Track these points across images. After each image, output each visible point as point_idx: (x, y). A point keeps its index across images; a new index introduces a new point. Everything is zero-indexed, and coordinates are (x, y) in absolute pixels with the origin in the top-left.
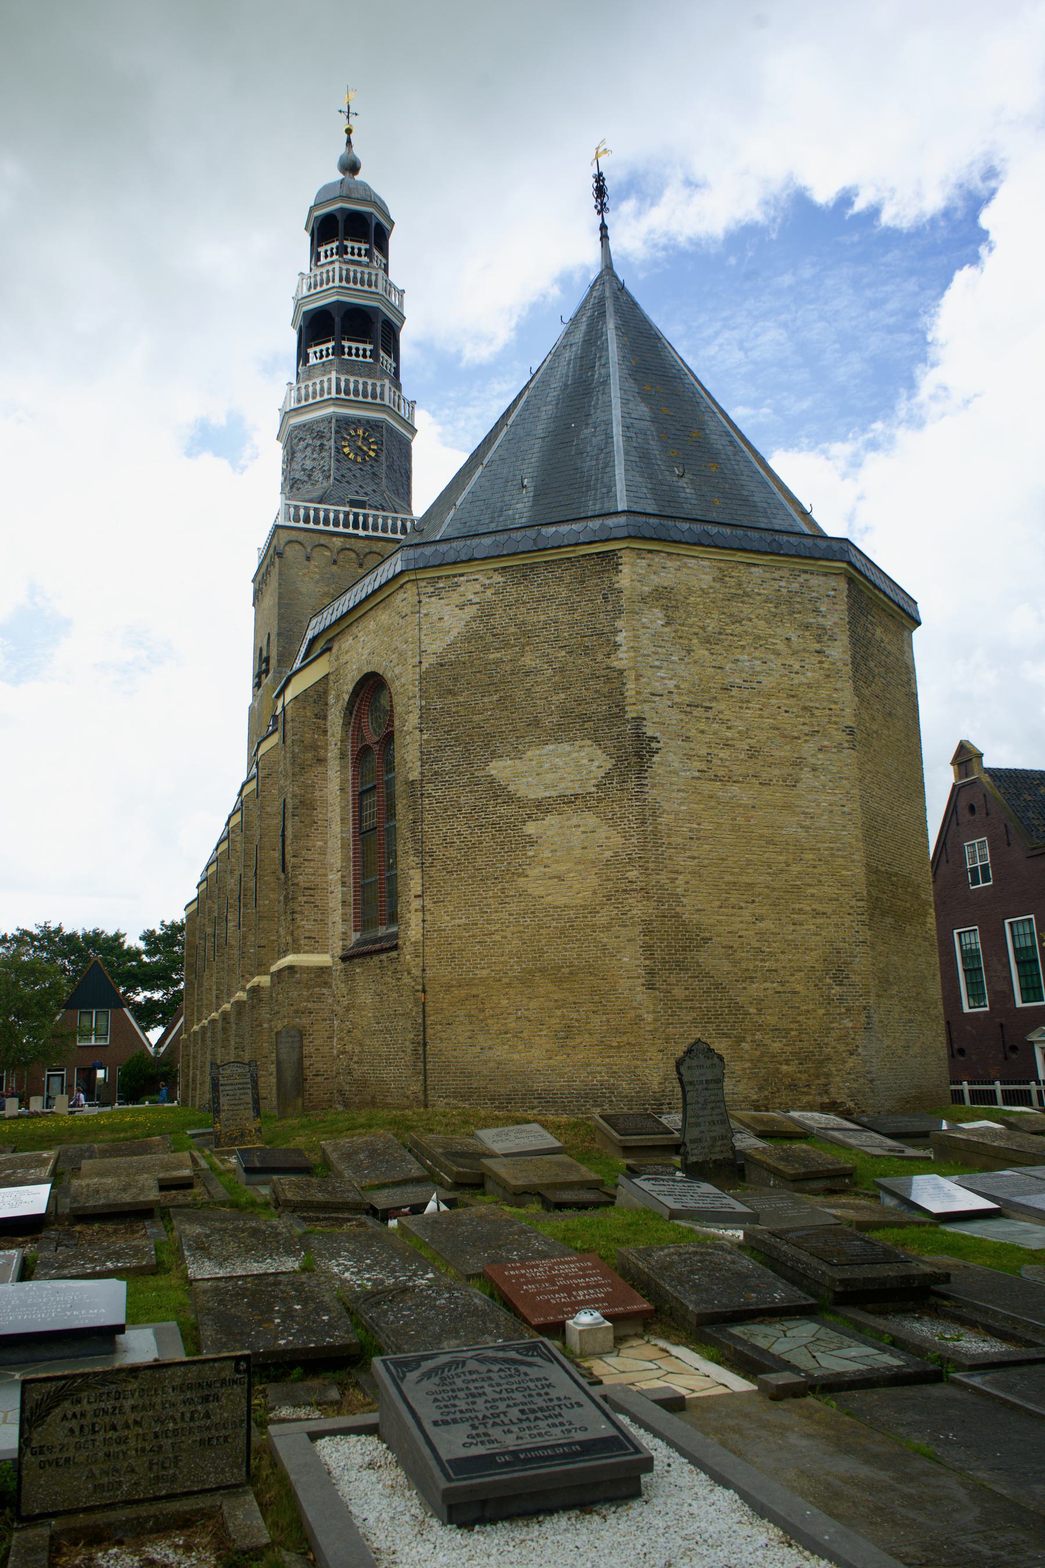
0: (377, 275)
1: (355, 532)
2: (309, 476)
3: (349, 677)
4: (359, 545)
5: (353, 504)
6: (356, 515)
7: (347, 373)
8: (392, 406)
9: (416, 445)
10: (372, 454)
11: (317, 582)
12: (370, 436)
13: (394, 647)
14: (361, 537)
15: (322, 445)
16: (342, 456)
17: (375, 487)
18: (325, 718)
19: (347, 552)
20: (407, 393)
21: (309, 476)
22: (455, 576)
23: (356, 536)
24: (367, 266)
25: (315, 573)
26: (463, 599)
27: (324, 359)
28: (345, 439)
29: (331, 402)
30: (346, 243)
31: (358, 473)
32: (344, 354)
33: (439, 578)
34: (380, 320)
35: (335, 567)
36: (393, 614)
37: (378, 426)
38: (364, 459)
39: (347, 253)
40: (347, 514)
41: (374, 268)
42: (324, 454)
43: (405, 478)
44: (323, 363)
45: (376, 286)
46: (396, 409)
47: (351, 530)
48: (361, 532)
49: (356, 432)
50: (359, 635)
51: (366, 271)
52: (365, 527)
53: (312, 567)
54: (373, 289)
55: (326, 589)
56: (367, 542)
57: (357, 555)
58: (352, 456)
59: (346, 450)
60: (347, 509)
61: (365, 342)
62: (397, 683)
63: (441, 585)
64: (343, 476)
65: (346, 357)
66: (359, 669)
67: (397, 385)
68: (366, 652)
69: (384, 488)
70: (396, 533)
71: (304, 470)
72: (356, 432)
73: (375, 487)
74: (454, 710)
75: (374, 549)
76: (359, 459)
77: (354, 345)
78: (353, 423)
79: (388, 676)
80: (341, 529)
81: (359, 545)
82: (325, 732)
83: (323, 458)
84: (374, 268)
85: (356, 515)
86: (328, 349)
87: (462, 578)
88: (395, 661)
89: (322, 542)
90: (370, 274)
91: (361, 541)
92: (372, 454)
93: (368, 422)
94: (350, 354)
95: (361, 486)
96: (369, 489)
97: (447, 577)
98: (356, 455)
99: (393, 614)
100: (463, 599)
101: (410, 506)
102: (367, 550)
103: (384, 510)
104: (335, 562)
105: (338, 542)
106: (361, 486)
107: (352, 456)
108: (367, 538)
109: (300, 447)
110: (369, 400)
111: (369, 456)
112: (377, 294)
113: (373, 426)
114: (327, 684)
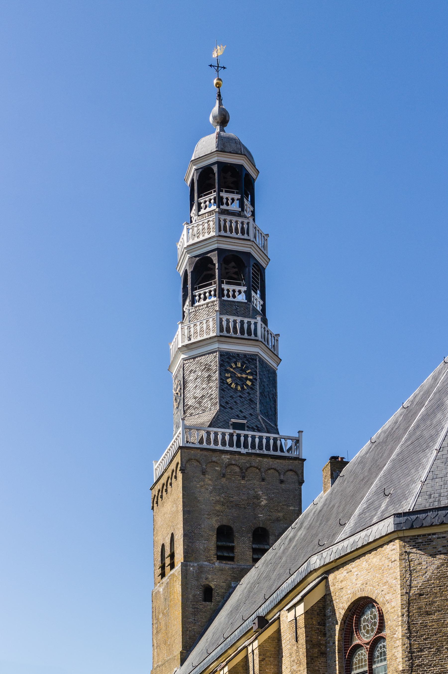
0: (248, 224)
1: (238, 450)
2: (200, 403)
3: (345, 598)
4: (243, 460)
5: (236, 426)
6: (239, 436)
7: (234, 315)
8: (263, 341)
9: (280, 372)
10: (249, 383)
11: (211, 492)
12: (247, 368)
13: (385, 581)
14: (243, 454)
15: (209, 376)
16: (226, 385)
17: (251, 411)
18: (324, 625)
19: (233, 467)
20: (273, 328)
21: (200, 403)
22: (429, 535)
23: (239, 453)
24: (239, 214)
25: (209, 485)
26: (435, 550)
27: (208, 300)
28: (228, 371)
29: (216, 339)
30: (222, 194)
31: (238, 400)
32: (224, 296)
33: (419, 536)
34: (252, 263)
35: (224, 480)
36: (384, 559)
37: (253, 359)
38: (242, 388)
39: (222, 204)
40: (231, 435)
41: (245, 217)
42: (211, 384)
43: (273, 402)
44: (207, 304)
45: (248, 234)
46: (266, 343)
47: (235, 449)
48: (243, 451)
49: (236, 364)
50: (353, 570)
51: (240, 220)
52: (246, 446)
53: (207, 480)
54: (246, 236)
55: (218, 498)
56: (248, 458)
57: (241, 469)
58: (233, 386)
59: (229, 380)
60: (231, 431)
61: (239, 285)
62: (388, 605)
63: (420, 541)
64: (227, 403)
65: (225, 298)
66: (354, 594)
67: (265, 321)
68: (359, 582)
69: (258, 411)
70: (277, 451)
71: (195, 398)
72: (236, 364)
73: (251, 411)
74: (430, 624)
75: (254, 464)
76: (239, 388)
77: (231, 287)
78: (234, 357)
79: (380, 600)
80: (227, 448)
81: (243, 460)
82: (325, 635)
83: (211, 388)
84: (245, 217)
85: (239, 436)
86: (210, 292)
87: (434, 536)
88: (385, 591)
89: (214, 459)
90: (242, 223)
91: (243, 457)
92: (249, 383)
93: (245, 355)
94: (228, 296)
95: (241, 411)
96: (246, 413)
97: (424, 535)
98: (237, 384)
99: (384, 559)
100: (435, 550)
101: (276, 425)
102: (248, 465)
103: (259, 431)
104: (224, 476)
105: (226, 458)
106: (241, 411)
107: (233, 386)
108: (248, 454)
109: (191, 378)
110: (246, 336)
111: (247, 385)
112: (249, 240)
113: (250, 359)
114: (325, 602)
